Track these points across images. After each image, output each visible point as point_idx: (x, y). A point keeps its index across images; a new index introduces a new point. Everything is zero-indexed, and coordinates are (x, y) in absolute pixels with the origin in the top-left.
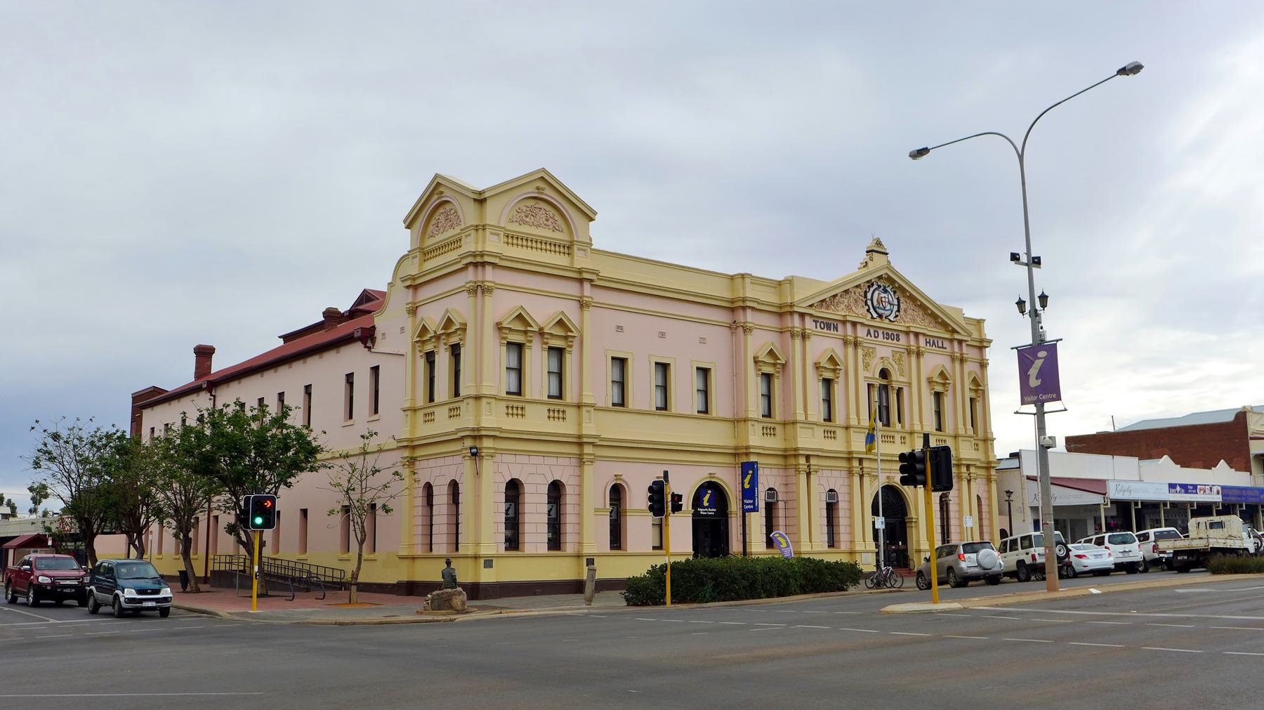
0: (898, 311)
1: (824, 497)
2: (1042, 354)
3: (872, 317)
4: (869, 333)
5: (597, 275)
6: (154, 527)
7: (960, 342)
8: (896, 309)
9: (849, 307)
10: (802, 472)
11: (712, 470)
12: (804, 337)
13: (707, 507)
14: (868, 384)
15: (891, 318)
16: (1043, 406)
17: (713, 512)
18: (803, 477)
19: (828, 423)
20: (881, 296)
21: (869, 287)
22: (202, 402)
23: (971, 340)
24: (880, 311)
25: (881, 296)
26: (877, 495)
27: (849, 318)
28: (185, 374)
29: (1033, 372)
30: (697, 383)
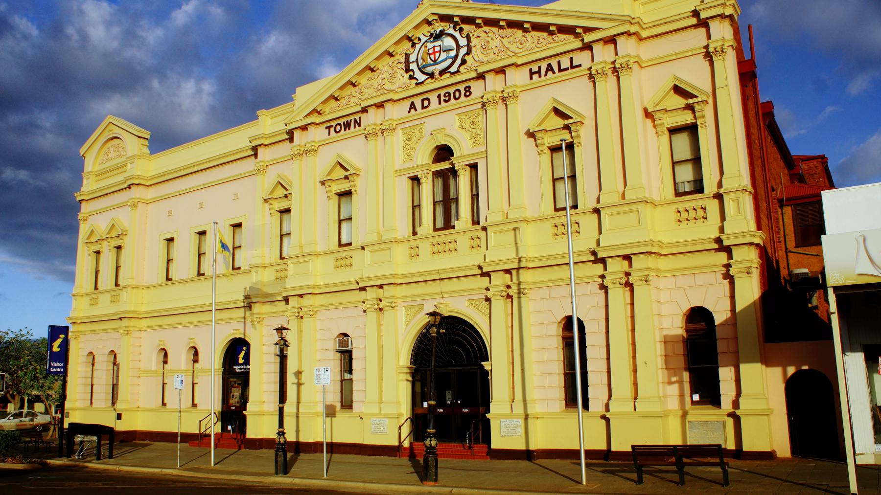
24: (429, 70)
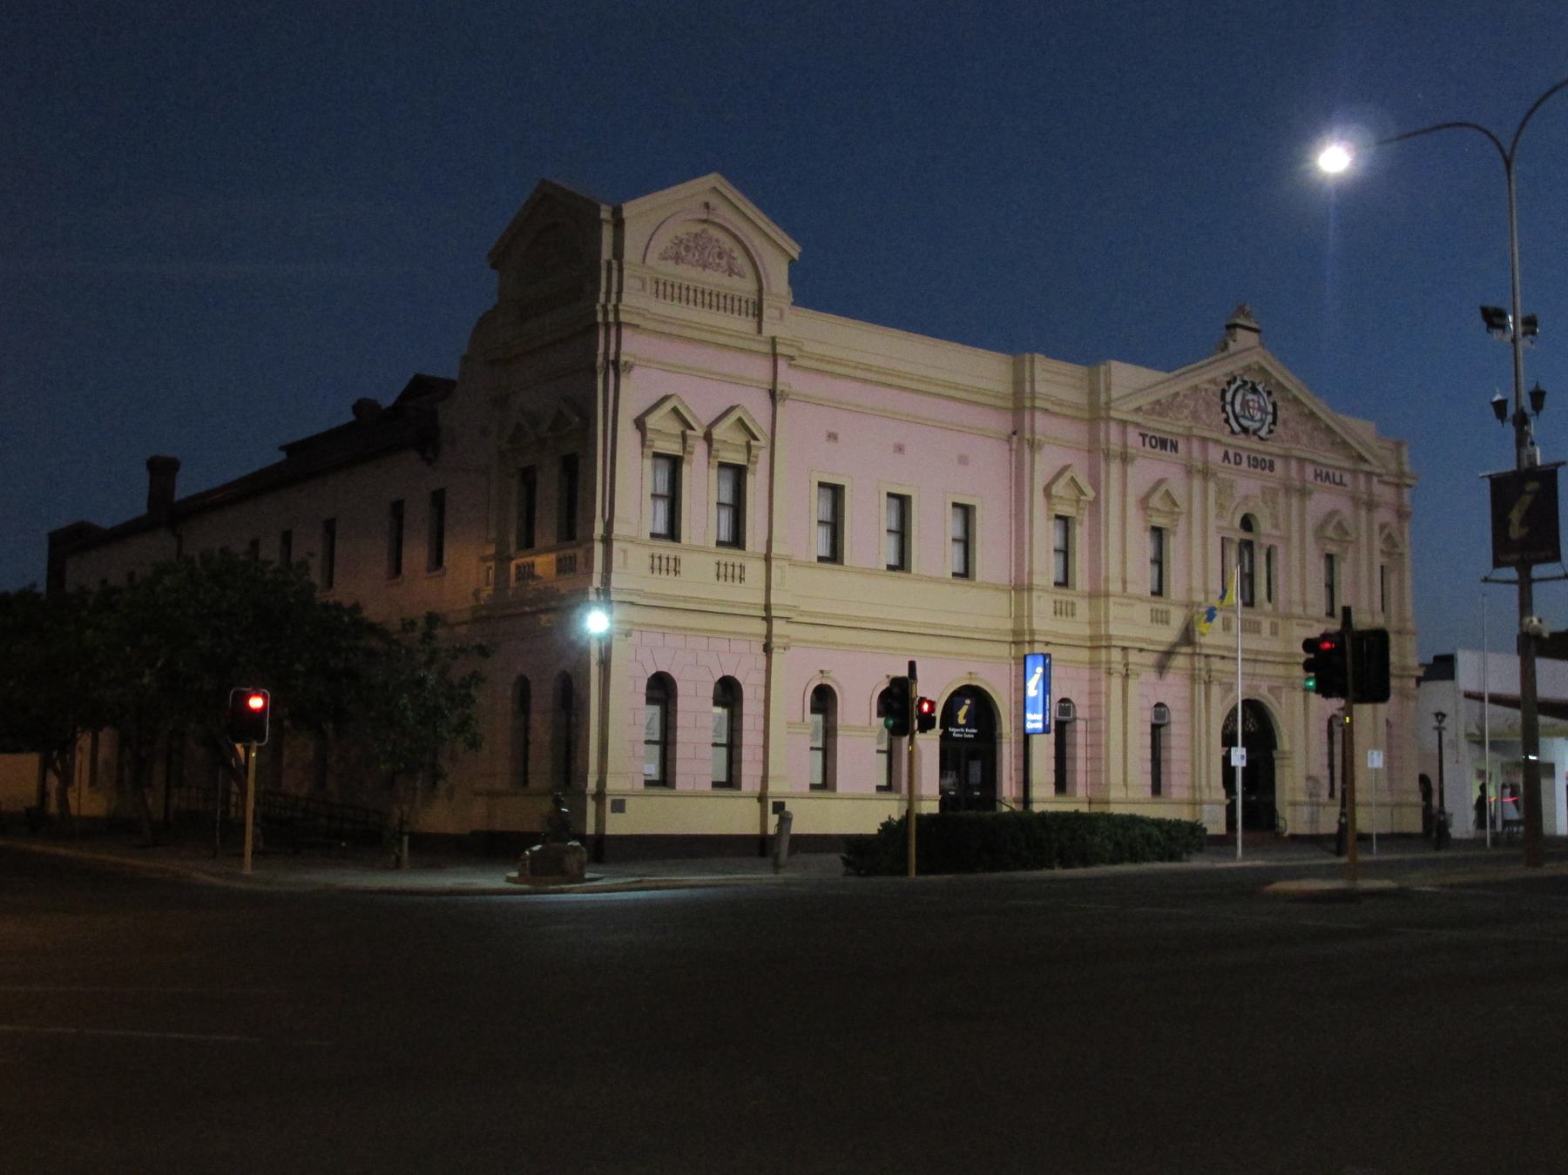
0: (1274, 422)
1: (1148, 716)
2: (1532, 486)
3: (1233, 432)
4: (1226, 456)
5: (799, 349)
6: (85, 741)
7: (1369, 474)
8: (1271, 421)
9: (1195, 416)
10: (1115, 675)
11: (973, 667)
12: (1125, 459)
13: (964, 726)
14: (1223, 539)
15: (1263, 433)
16: (1529, 569)
17: (972, 733)
18: (1116, 682)
19: (1155, 598)
20: (1247, 398)
21: (1229, 383)
22: (156, 548)
23: (1387, 474)
24: (1245, 422)
25: (1247, 398)
26: (1235, 709)
27: (1195, 432)
28: (135, 505)
29: (1515, 516)
30: (954, 527)
